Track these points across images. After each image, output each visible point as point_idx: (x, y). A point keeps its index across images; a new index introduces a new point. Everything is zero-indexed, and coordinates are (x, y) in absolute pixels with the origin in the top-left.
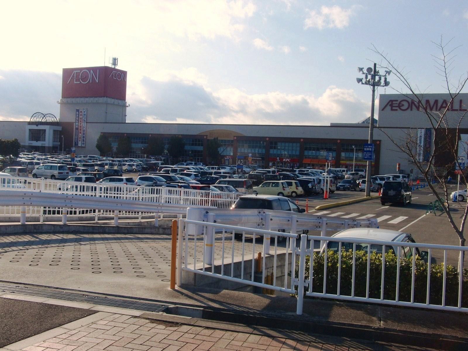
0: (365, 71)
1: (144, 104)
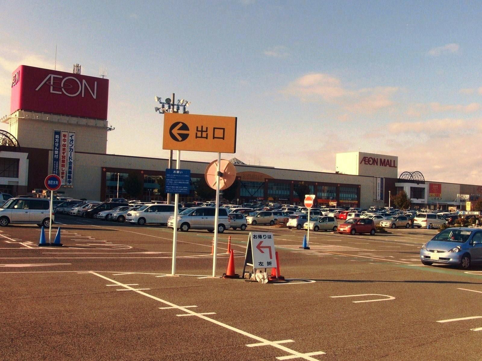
0: (163, 101)
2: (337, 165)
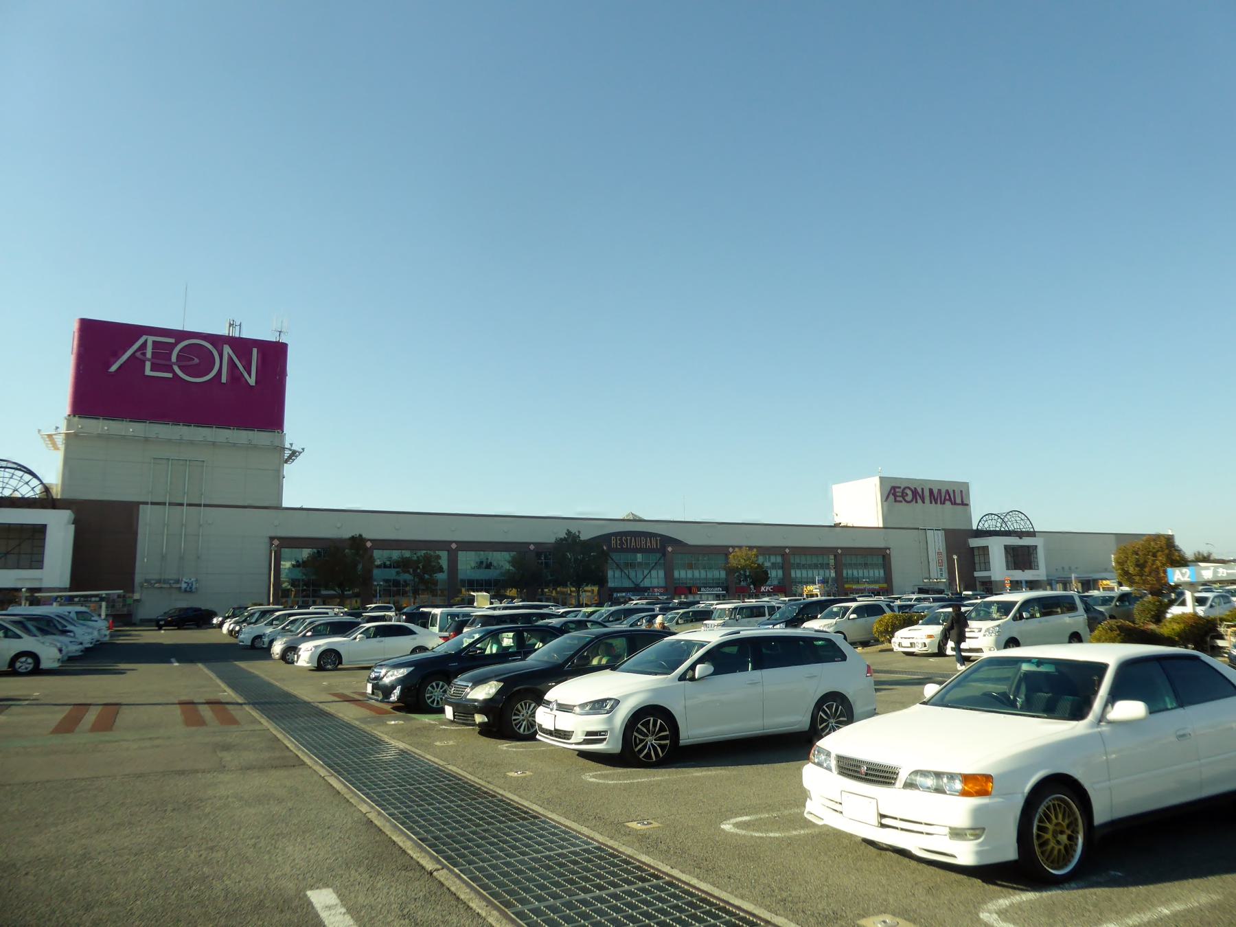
2: (836, 510)
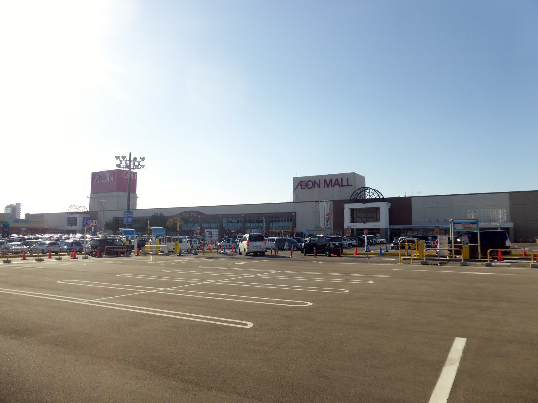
1: (152, 195)
